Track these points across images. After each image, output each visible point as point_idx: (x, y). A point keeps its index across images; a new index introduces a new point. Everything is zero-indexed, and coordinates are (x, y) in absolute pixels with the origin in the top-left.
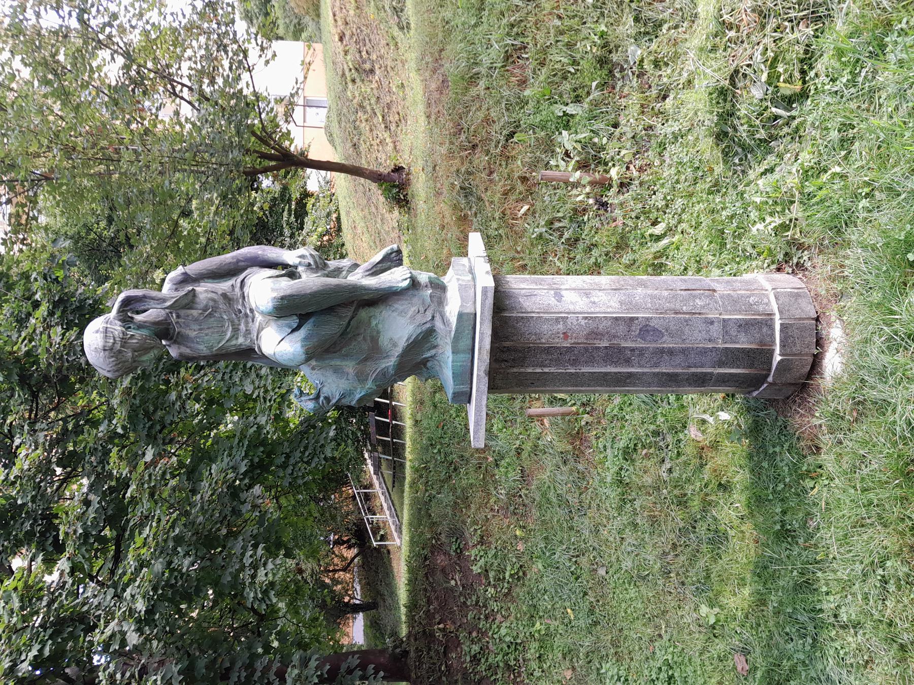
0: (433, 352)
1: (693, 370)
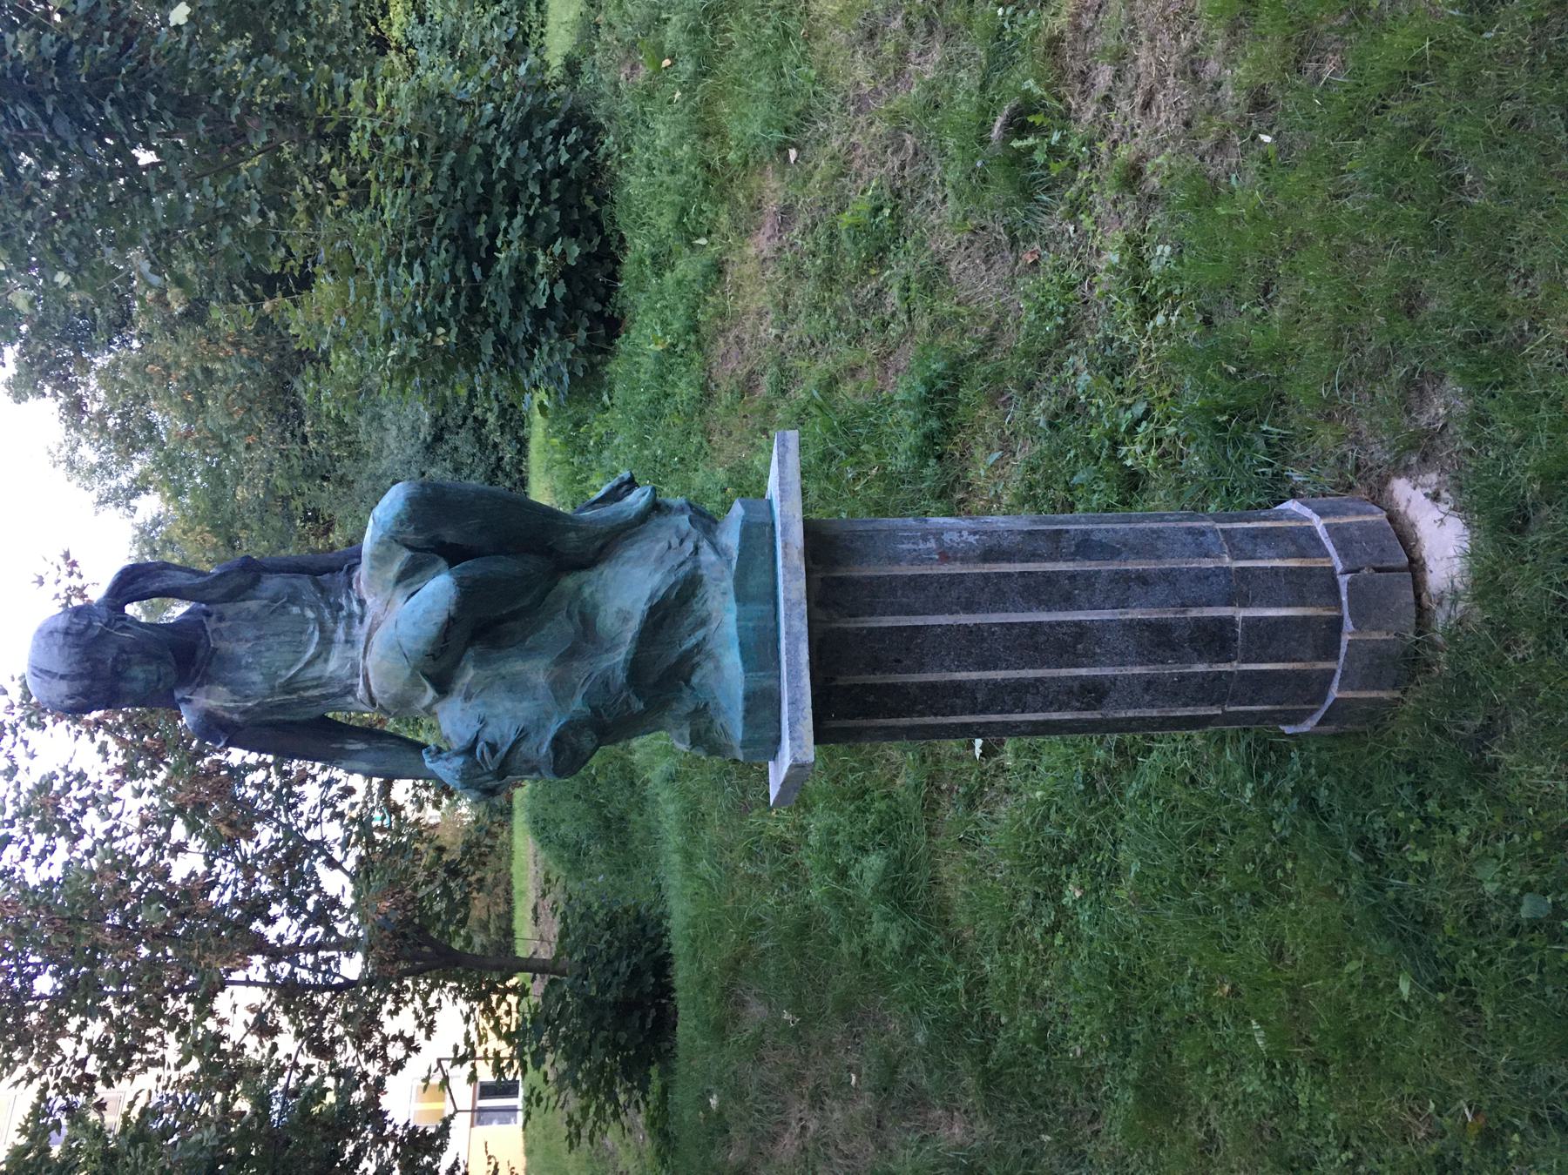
0: (700, 634)
1: (1194, 613)
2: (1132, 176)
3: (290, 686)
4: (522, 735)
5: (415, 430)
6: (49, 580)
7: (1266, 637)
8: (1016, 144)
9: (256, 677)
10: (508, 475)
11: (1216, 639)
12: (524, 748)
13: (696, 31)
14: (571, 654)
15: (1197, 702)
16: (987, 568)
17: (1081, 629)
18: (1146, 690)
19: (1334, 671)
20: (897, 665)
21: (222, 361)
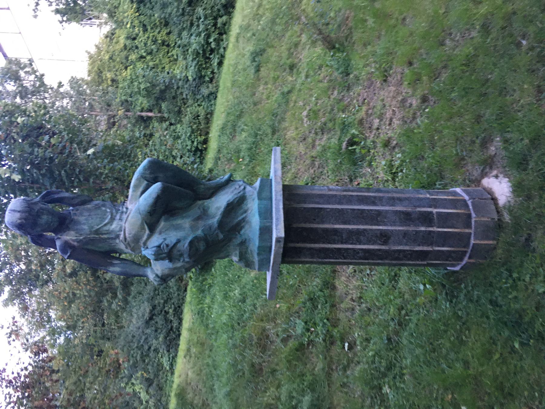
0: (244, 215)
1: (419, 209)
2: (387, 144)
3: (97, 232)
4: (179, 241)
5: (143, 315)
6: (5, 327)
7: (444, 219)
8: (350, 148)
9: (86, 227)
10: (174, 333)
11: (427, 219)
12: (178, 245)
13: (250, 149)
14: (199, 218)
15: (423, 244)
16: (345, 193)
17: (379, 213)
18: (404, 237)
19: (470, 234)
20: (314, 221)
21: (80, 290)
